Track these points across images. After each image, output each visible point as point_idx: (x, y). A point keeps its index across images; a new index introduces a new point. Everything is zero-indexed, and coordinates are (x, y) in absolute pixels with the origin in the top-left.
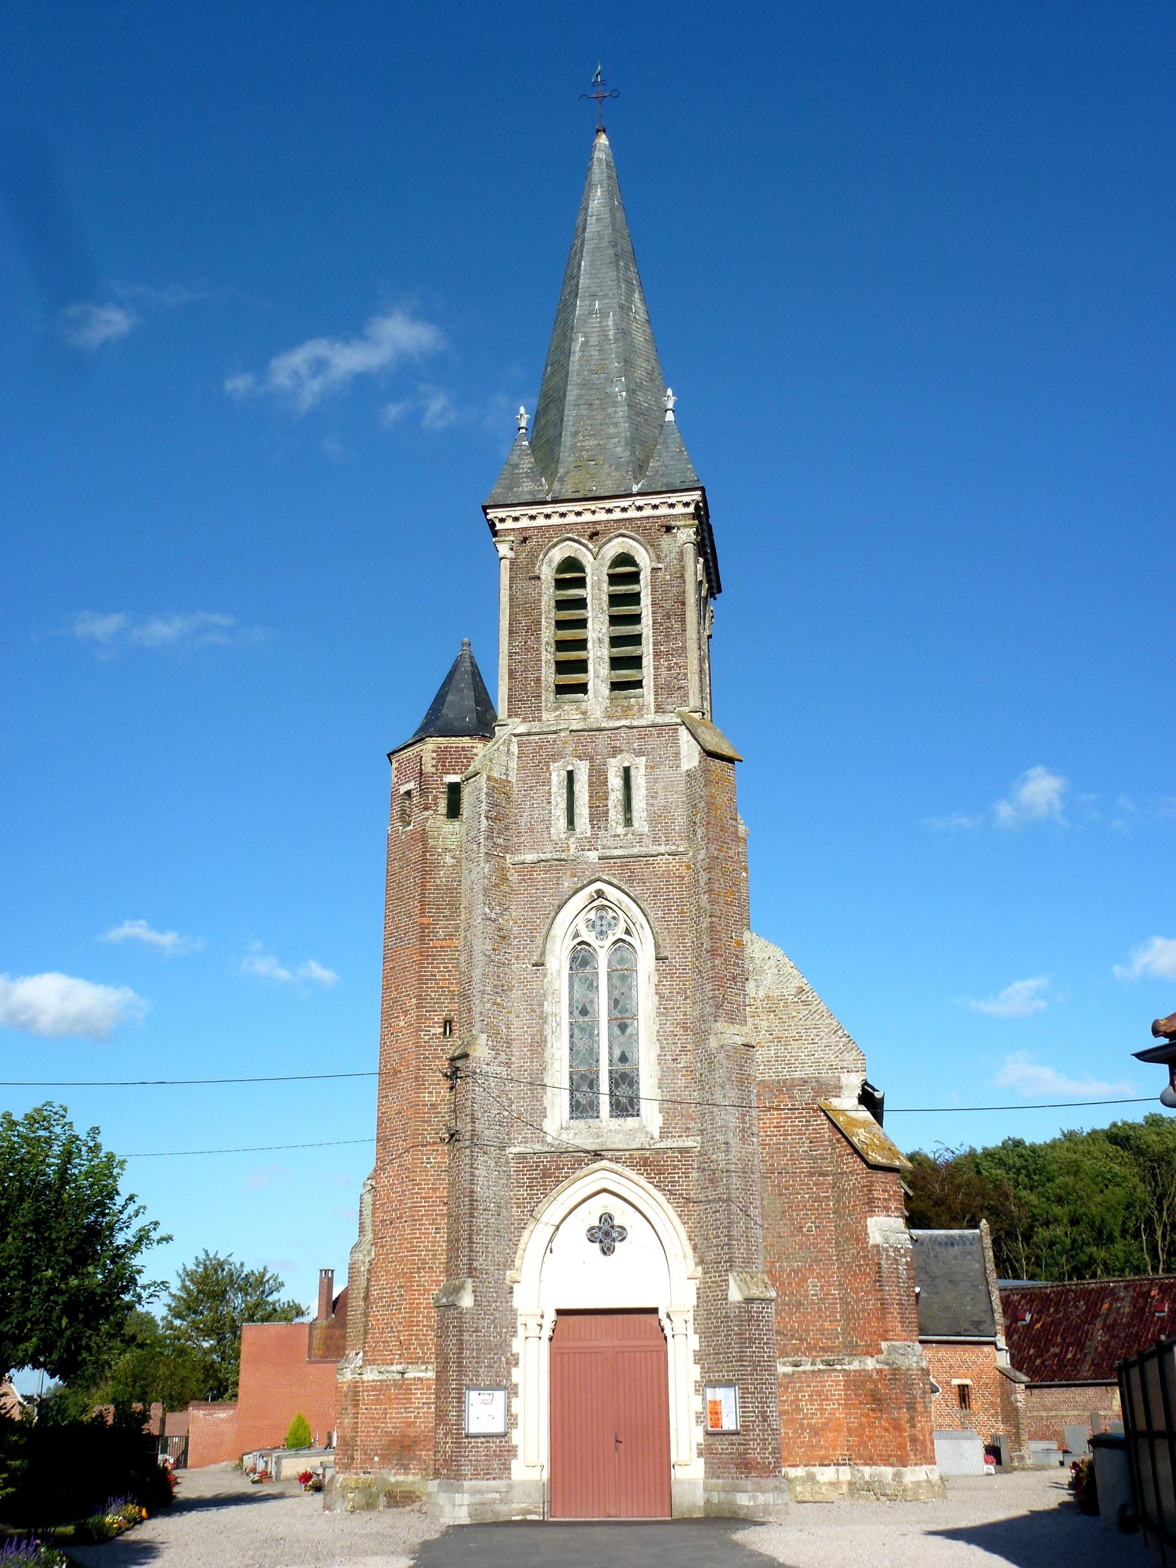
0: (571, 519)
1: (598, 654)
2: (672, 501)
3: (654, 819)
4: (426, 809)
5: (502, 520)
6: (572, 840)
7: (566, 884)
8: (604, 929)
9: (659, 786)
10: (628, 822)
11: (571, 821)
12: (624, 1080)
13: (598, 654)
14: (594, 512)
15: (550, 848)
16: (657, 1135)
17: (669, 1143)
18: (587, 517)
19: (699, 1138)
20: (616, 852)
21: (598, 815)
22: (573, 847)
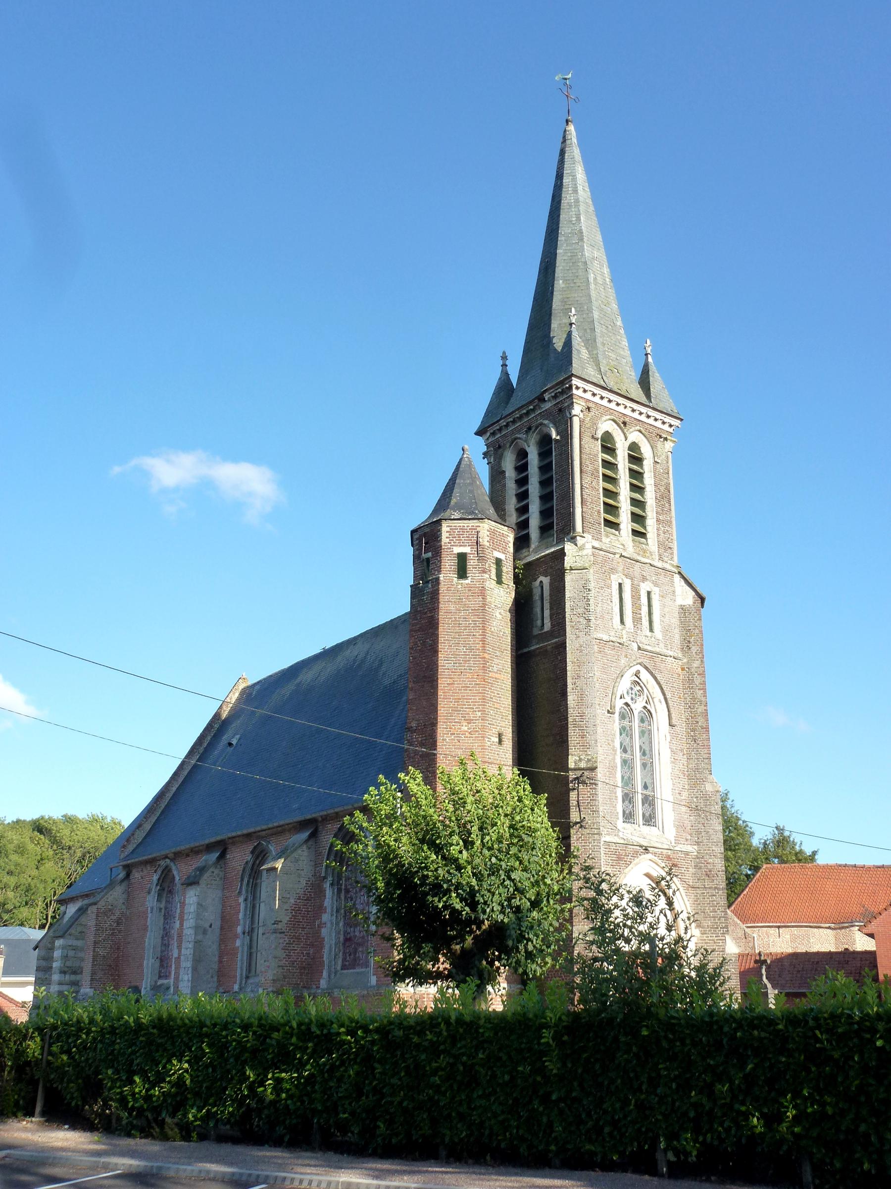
0: (613, 406)
1: (625, 509)
2: (666, 420)
3: (666, 631)
4: (484, 572)
5: (577, 388)
6: (624, 632)
7: (623, 661)
8: (633, 696)
9: (666, 610)
10: (651, 630)
11: (622, 622)
12: (649, 801)
13: (625, 509)
14: (664, 423)
15: (612, 634)
16: (673, 842)
17: (602, 843)
18: (621, 409)
19: (696, 847)
20: (649, 648)
21: (637, 620)
22: (625, 636)
